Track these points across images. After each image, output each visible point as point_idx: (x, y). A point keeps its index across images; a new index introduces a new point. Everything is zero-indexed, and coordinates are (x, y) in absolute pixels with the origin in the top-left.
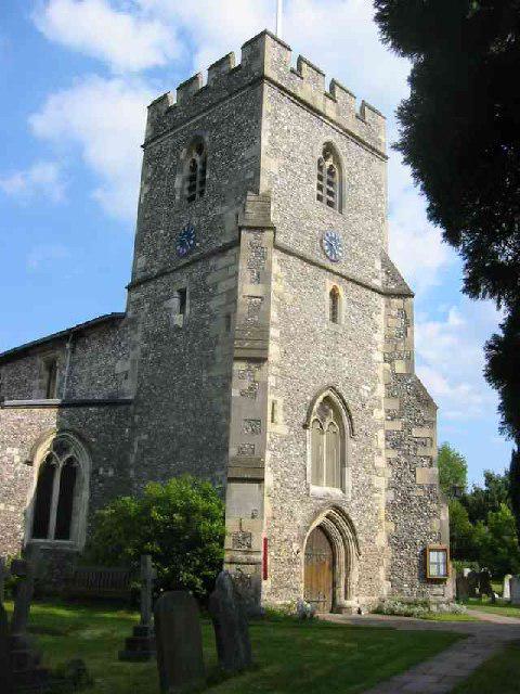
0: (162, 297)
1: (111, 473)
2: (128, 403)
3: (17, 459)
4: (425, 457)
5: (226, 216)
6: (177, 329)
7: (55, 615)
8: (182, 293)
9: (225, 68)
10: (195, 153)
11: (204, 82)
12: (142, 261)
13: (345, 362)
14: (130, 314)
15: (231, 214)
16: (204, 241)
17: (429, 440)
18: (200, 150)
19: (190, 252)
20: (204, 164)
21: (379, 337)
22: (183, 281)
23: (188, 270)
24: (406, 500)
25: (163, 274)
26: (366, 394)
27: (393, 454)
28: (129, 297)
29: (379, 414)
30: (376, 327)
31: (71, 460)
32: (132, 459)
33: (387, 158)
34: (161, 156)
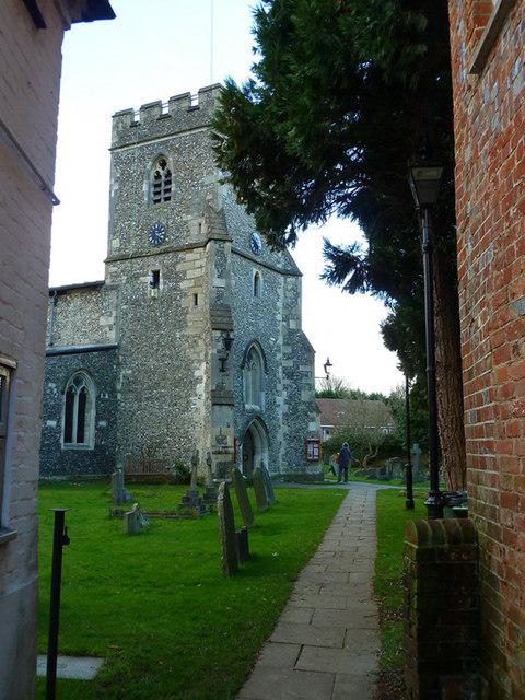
2: (114, 348)
3: (55, 391)
6: (154, 299)
8: (156, 274)
12: (116, 243)
13: (261, 324)
15: (195, 222)
18: (163, 164)
19: (160, 244)
21: (279, 304)
23: (161, 258)
24: (295, 410)
27: (287, 382)
28: (107, 270)
29: (279, 356)
32: (119, 387)
34: (130, 162)
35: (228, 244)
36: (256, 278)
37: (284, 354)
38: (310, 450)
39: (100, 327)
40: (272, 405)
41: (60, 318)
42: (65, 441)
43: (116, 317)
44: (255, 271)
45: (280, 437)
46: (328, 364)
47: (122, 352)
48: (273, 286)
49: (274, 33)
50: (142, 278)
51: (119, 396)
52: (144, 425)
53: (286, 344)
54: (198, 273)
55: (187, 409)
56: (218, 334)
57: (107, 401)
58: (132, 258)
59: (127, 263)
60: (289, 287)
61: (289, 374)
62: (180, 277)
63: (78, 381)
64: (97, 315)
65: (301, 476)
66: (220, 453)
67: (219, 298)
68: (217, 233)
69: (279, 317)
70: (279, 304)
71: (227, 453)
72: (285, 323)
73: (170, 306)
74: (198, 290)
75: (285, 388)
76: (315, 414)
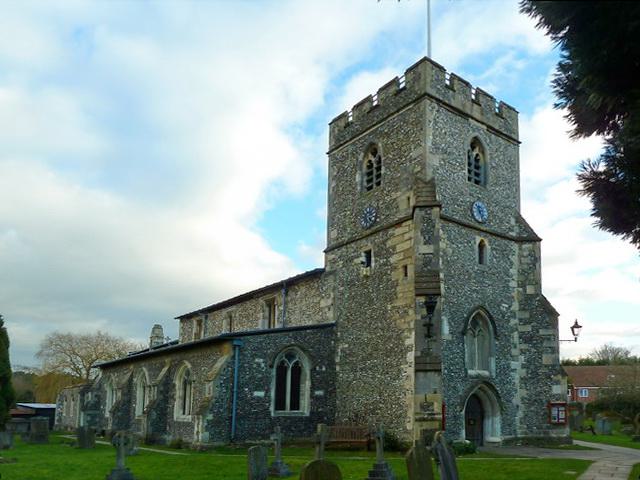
1: (324, 369)
2: (332, 325)
3: (263, 365)
5: (399, 200)
6: (366, 277)
8: (368, 254)
10: (370, 155)
12: (334, 234)
13: (489, 291)
14: (328, 269)
15: (404, 197)
18: (375, 153)
19: (371, 226)
20: (379, 162)
21: (513, 271)
22: (368, 245)
27: (524, 346)
28: (326, 258)
32: (337, 360)
35: (437, 209)
36: (481, 246)
37: (521, 320)
38: (554, 412)
39: (321, 309)
40: (505, 370)
41: (290, 305)
42: (276, 409)
43: (334, 298)
44: (478, 239)
45: (516, 400)
46: (576, 326)
47: (339, 329)
48: (505, 254)
49: (611, 363)
50: (356, 261)
51: (338, 368)
52: (357, 396)
53: (522, 309)
54: (406, 245)
55: (397, 377)
56: (422, 300)
57: (324, 372)
58: (347, 243)
59: (344, 249)
60: (525, 254)
61: (526, 338)
62: (390, 252)
63: (290, 356)
64: (318, 299)
65: (543, 439)
66: (424, 420)
67: (426, 264)
68: (424, 199)
69: (513, 284)
70: (513, 271)
71: (433, 420)
72: (521, 289)
73: (381, 281)
74: (408, 262)
75: (522, 352)
76: (560, 377)
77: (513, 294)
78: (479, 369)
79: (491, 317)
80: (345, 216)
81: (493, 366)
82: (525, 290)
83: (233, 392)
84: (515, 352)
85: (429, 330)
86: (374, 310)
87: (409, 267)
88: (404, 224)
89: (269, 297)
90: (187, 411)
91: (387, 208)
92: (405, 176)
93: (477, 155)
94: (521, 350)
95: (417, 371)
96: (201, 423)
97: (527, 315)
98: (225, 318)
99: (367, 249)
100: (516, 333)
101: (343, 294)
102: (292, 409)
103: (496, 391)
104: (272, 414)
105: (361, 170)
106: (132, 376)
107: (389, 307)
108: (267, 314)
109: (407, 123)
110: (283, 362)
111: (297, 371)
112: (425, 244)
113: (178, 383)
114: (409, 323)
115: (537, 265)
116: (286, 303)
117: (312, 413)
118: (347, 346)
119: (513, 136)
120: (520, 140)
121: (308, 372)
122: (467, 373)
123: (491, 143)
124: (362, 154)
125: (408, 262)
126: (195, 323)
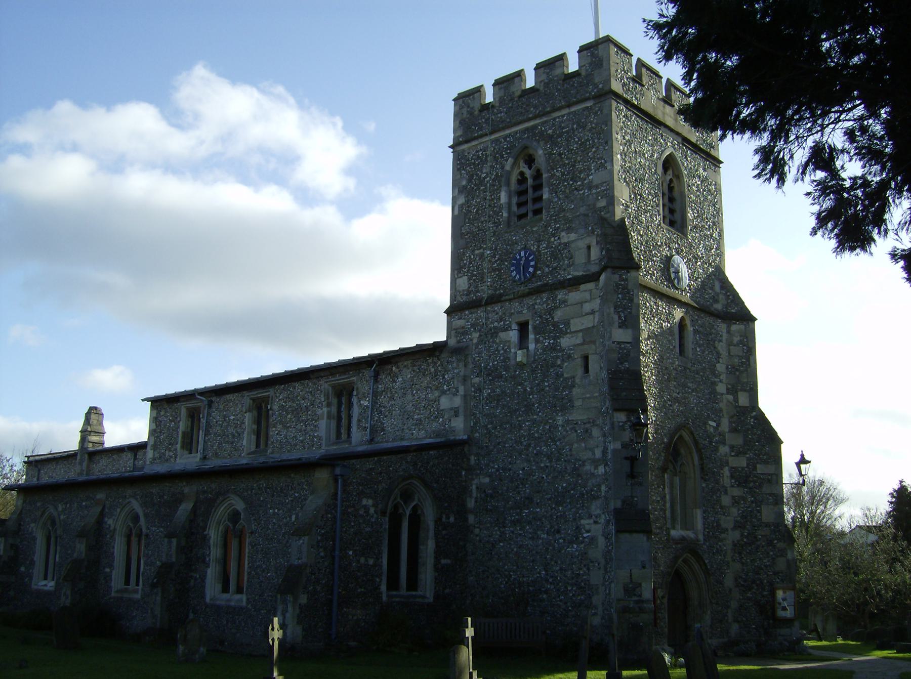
0: (495, 328)
1: (452, 519)
2: (462, 443)
3: (372, 510)
4: (770, 495)
5: (573, 245)
6: (521, 366)
7: (829, 641)
8: (523, 328)
9: (558, 72)
10: (522, 164)
11: (530, 81)
14: (453, 343)
15: (582, 244)
16: (547, 270)
17: (774, 477)
20: (538, 175)
21: (720, 367)
22: (521, 310)
25: (493, 300)
26: (712, 430)
27: (737, 492)
30: (719, 355)
31: (415, 509)
32: (471, 504)
33: (632, 56)
37: (732, 447)
39: (440, 413)
42: (389, 588)
46: (803, 461)
51: (471, 519)
59: (480, 312)
60: (736, 339)
63: (407, 496)
64: (437, 394)
69: (721, 388)
70: (720, 367)
72: (730, 397)
74: (590, 349)
77: (721, 405)
78: (682, 529)
79: (696, 443)
80: (482, 256)
81: (699, 525)
82: (736, 400)
83: (333, 557)
84: (726, 500)
85: (632, 467)
86: (534, 422)
87: (592, 359)
88: (583, 287)
89: (341, 379)
90: (233, 586)
91: (554, 256)
92: (582, 210)
93: (671, 181)
94: (733, 497)
95: (618, 531)
96: (290, 609)
97: (738, 440)
98: (249, 410)
99: (522, 319)
100: (727, 468)
101: (479, 390)
102: (408, 589)
103: (705, 564)
104: (384, 598)
105: (508, 184)
106: (102, 514)
107: (560, 420)
108: (334, 410)
109: (584, 127)
110: (396, 507)
111: (416, 520)
112: (620, 327)
113: (214, 534)
114: (592, 450)
115: (751, 361)
116: (376, 394)
117: (437, 597)
118: (487, 480)
119: (713, 152)
120: (721, 159)
121: (431, 525)
122: (668, 534)
123: (688, 162)
124: (511, 160)
125: (590, 349)
126: (184, 412)
